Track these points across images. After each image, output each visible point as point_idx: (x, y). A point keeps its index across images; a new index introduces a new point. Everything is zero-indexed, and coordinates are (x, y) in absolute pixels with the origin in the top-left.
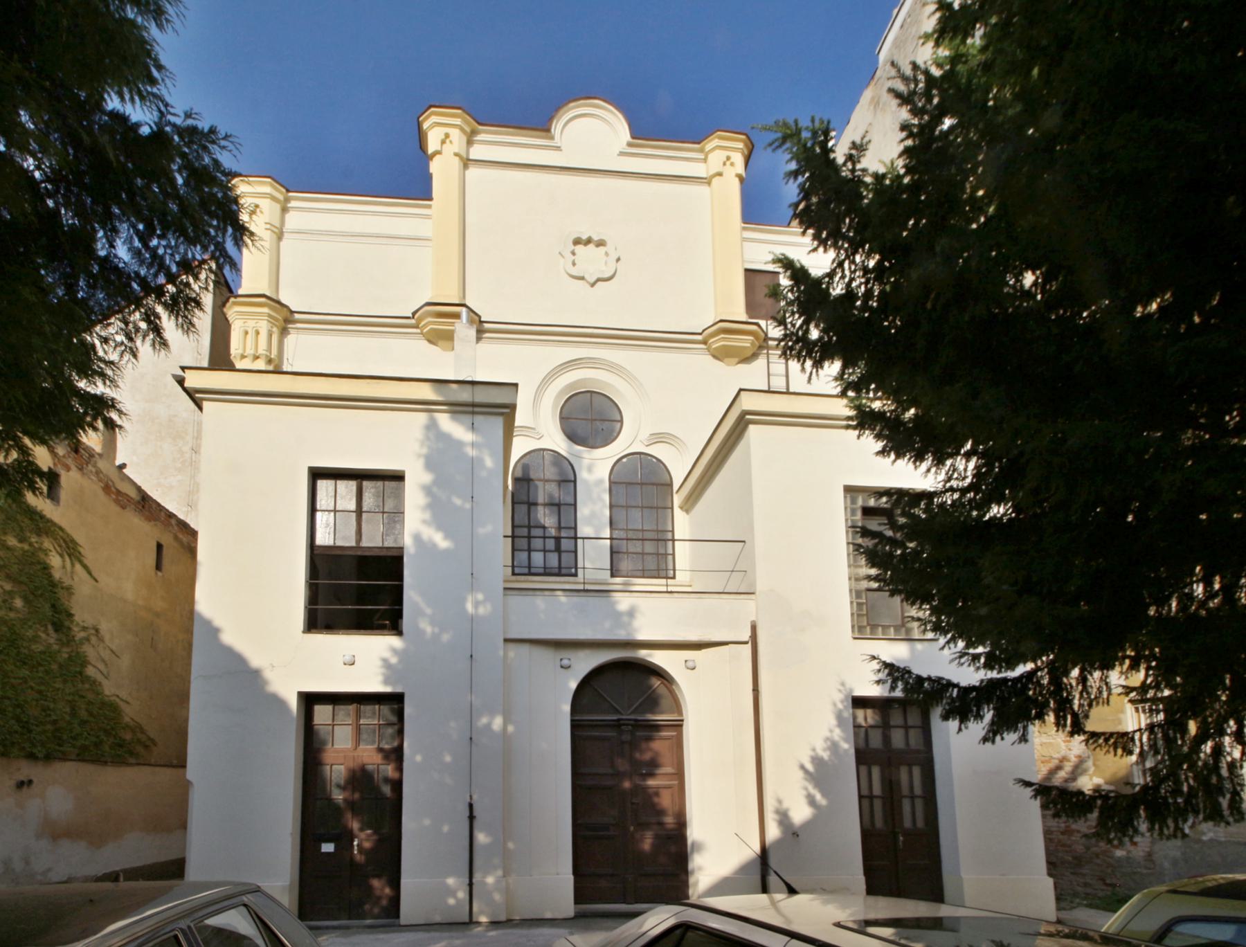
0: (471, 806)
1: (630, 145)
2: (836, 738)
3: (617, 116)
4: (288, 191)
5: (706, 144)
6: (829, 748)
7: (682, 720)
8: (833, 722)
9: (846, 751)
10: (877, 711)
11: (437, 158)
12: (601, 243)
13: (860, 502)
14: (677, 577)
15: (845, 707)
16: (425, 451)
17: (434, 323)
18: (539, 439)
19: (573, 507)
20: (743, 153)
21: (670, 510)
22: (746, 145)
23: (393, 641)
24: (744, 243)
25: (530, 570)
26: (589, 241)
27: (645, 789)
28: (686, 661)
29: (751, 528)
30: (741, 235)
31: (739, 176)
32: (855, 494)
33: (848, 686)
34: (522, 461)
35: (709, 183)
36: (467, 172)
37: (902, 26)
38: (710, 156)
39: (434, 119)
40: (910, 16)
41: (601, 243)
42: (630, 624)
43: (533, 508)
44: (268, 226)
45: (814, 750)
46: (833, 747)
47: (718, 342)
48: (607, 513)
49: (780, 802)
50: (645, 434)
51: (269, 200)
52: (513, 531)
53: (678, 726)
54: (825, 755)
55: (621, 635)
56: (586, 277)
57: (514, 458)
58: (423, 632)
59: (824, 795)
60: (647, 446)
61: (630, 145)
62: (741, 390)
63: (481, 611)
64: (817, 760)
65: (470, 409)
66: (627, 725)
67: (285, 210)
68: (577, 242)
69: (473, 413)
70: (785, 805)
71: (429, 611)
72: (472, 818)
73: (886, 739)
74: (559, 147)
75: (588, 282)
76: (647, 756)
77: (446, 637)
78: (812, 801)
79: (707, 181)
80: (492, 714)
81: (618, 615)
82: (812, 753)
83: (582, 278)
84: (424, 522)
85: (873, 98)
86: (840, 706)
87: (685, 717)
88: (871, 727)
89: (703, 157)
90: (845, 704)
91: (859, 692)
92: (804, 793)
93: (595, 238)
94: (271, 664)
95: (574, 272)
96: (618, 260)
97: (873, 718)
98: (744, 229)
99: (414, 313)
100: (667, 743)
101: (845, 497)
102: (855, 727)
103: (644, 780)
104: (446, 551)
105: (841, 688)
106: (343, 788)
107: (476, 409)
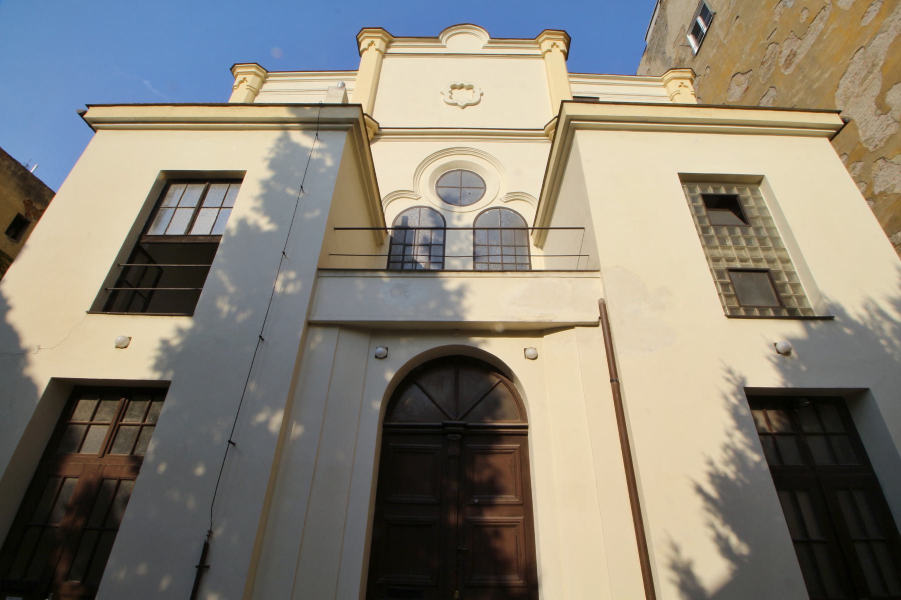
0: (206, 548)
1: (489, 42)
2: (740, 446)
3: (482, 32)
4: (267, 72)
5: (539, 38)
6: (732, 461)
7: (526, 427)
8: (730, 422)
9: (757, 464)
10: (781, 412)
11: (365, 52)
12: (470, 88)
13: (698, 191)
15: (740, 401)
16: (272, 155)
18: (417, 199)
19: (442, 247)
20: (564, 41)
22: (565, 37)
23: (185, 322)
24: (571, 84)
26: (462, 87)
27: (480, 526)
28: (525, 349)
29: (588, 213)
30: (568, 80)
31: (563, 51)
32: (692, 185)
33: (737, 374)
34: (404, 215)
35: (543, 58)
36: (384, 60)
37: (656, 24)
38: (543, 45)
39: (365, 35)
40: (659, 17)
42: (458, 303)
43: (407, 248)
44: (248, 87)
45: (711, 463)
46: (738, 458)
48: (472, 248)
49: (676, 549)
50: (503, 194)
51: (253, 75)
53: (521, 434)
54: (730, 471)
55: (448, 315)
56: (458, 103)
58: (219, 311)
59: (741, 537)
60: (505, 202)
61: (489, 42)
63: (290, 289)
64: (717, 479)
65: (316, 125)
66: (454, 433)
67: (264, 82)
68: (454, 87)
69: (318, 129)
70: (686, 554)
71: (231, 289)
72: (202, 568)
73: (805, 451)
74: (445, 46)
75: (460, 106)
76: (486, 475)
77: (242, 317)
78: (726, 550)
79: (542, 57)
80: (274, 409)
81: (446, 294)
82: (708, 468)
83: (456, 104)
84: (255, 209)
85: (647, 59)
86: (734, 400)
87: (529, 424)
88: (780, 434)
89: (538, 46)
90: (740, 397)
91: (754, 382)
92: (711, 533)
93: (466, 84)
94: (39, 346)
95: (451, 101)
96: (482, 95)
97: (779, 421)
98: (570, 76)
100: (508, 458)
101: (683, 187)
102: (760, 434)
103: (480, 514)
104: (269, 233)
105: (729, 376)
106: (69, 509)
107: (320, 125)
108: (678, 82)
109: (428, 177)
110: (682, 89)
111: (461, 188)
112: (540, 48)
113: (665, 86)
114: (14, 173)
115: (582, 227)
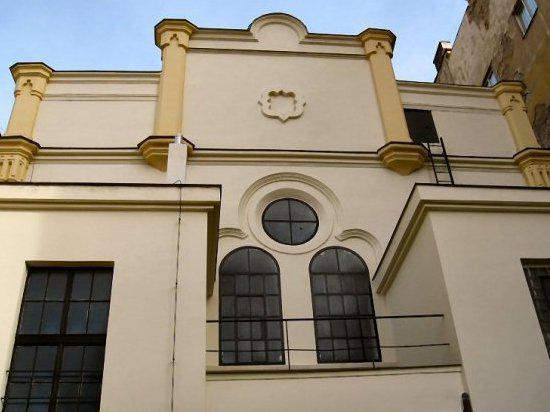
14: (383, 359)
17: (154, 151)
21: (374, 341)
25: (237, 357)
38: (367, 44)
41: (291, 95)
47: (391, 158)
50: (339, 231)
52: (220, 346)
57: (220, 257)
62: (416, 184)
69: (180, 211)
75: (281, 120)
99: (139, 145)
108: (510, 96)
109: (262, 196)
110: (514, 103)
111: (291, 222)
112: (363, 46)
113: (496, 97)
114: (444, 68)
115: (459, 401)
